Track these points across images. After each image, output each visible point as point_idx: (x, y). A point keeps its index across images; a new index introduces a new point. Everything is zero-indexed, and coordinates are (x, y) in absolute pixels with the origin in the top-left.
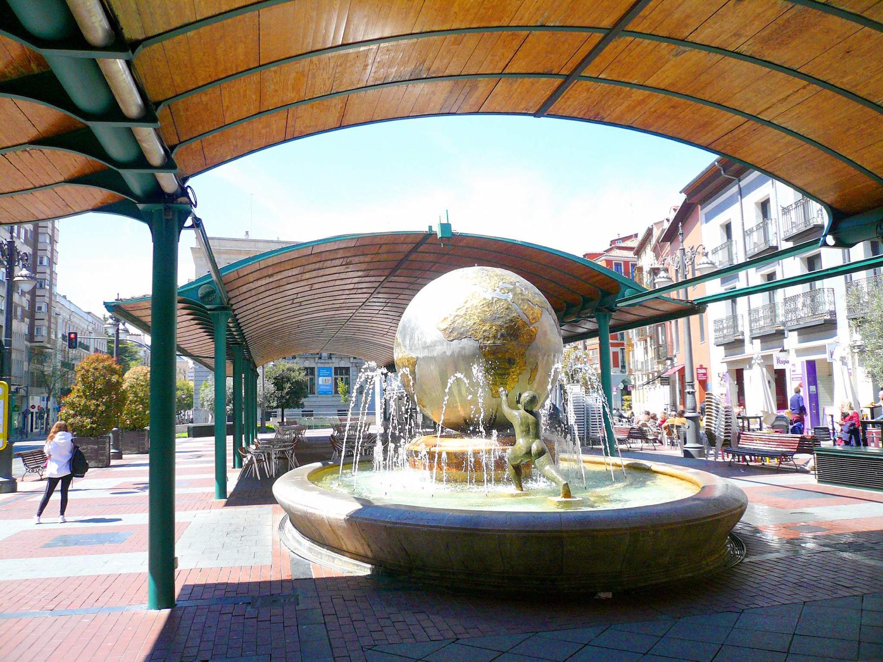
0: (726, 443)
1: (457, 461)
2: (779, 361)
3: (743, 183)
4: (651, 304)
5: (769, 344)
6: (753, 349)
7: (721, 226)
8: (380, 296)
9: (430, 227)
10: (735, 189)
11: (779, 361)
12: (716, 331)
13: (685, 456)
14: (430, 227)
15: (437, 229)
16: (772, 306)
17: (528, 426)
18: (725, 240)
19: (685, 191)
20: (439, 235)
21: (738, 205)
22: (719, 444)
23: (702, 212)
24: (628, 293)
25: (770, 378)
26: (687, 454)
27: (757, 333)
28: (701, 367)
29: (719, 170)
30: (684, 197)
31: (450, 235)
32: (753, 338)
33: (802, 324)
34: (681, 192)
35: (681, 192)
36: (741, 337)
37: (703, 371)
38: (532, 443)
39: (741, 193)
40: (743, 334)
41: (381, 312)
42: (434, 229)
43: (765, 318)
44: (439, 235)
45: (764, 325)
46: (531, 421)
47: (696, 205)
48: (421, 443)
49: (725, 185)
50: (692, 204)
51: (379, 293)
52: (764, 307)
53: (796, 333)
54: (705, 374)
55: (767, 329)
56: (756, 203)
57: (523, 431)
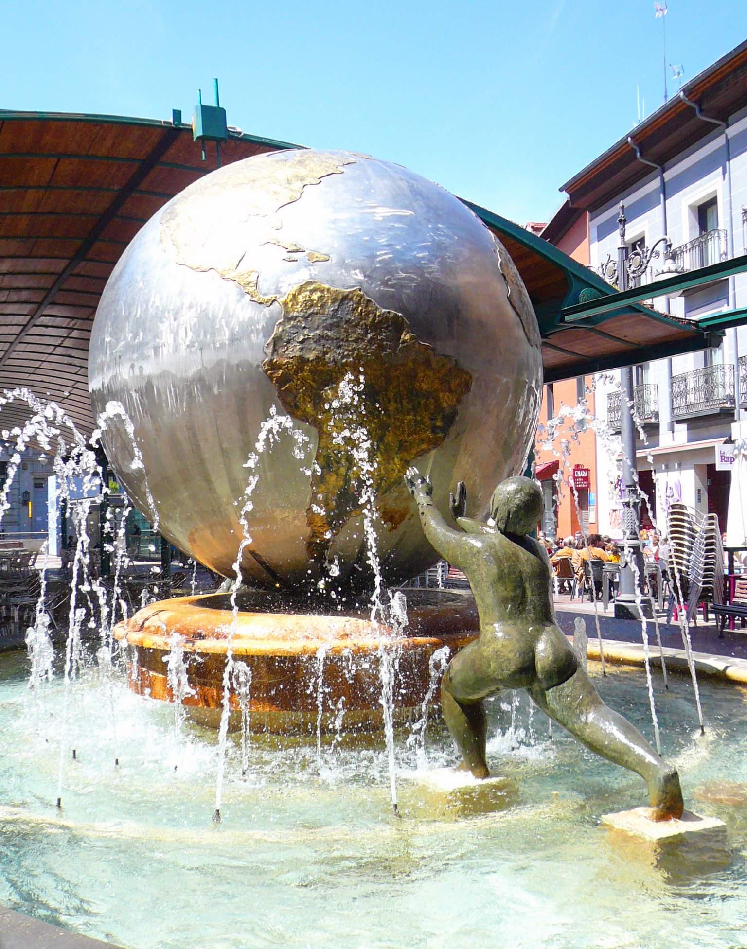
0: (705, 596)
1: (281, 679)
2: (723, 458)
3: (668, 175)
4: (611, 326)
5: (704, 432)
6: (677, 438)
7: (691, 207)
8: (55, 311)
9: (177, 114)
10: (655, 184)
11: (723, 458)
12: (610, 410)
13: (617, 616)
14: (177, 114)
15: (192, 120)
16: (708, 372)
17: (519, 584)
18: (697, 234)
19: (565, 188)
20: (198, 132)
21: (659, 209)
22: (693, 598)
23: (592, 225)
24: (585, 295)
25: (701, 486)
26: (623, 612)
27: (682, 413)
28: (578, 468)
29: (634, 151)
30: (565, 197)
31: (223, 135)
32: (678, 422)
33: (692, 413)
34: (561, 190)
35: (561, 190)
36: (653, 421)
37: (583, 474)
38: (535, 638)
39: (666, 191)
40: (657, 415)
41: (59, 350)
42: (185, 120)
43: (697, 389)
44: (198, 132)
45: (695, 401)
46: (526, 569)
47: (584, 211)
48: (165, 622)
49: (640, 176)
50: (575, 210)
51: (53, 304)
52: (696, 373)
53: (684, 426)
54: (586, 479)
55: (700, 408)
56: (690, 206)
57: (504, 601)
